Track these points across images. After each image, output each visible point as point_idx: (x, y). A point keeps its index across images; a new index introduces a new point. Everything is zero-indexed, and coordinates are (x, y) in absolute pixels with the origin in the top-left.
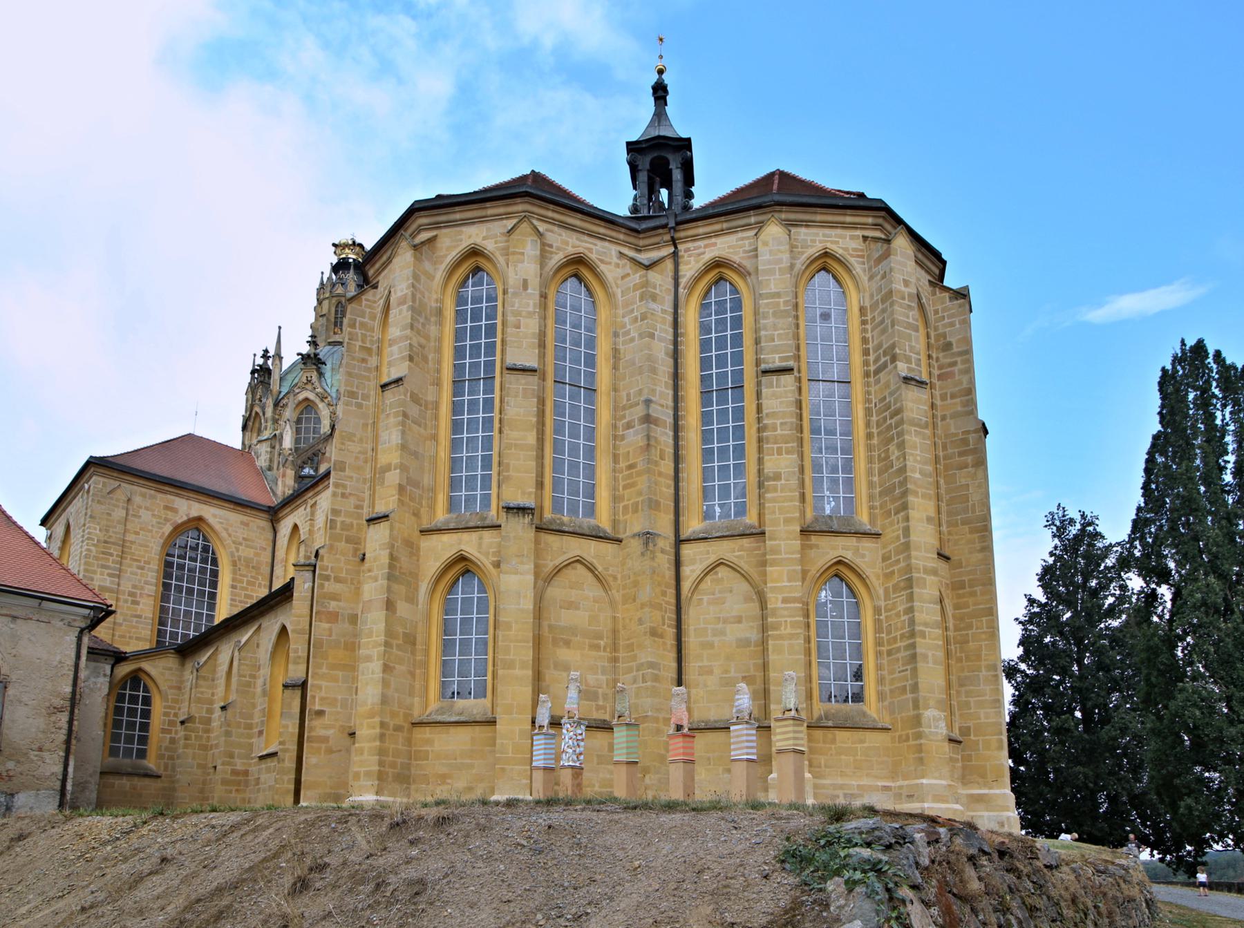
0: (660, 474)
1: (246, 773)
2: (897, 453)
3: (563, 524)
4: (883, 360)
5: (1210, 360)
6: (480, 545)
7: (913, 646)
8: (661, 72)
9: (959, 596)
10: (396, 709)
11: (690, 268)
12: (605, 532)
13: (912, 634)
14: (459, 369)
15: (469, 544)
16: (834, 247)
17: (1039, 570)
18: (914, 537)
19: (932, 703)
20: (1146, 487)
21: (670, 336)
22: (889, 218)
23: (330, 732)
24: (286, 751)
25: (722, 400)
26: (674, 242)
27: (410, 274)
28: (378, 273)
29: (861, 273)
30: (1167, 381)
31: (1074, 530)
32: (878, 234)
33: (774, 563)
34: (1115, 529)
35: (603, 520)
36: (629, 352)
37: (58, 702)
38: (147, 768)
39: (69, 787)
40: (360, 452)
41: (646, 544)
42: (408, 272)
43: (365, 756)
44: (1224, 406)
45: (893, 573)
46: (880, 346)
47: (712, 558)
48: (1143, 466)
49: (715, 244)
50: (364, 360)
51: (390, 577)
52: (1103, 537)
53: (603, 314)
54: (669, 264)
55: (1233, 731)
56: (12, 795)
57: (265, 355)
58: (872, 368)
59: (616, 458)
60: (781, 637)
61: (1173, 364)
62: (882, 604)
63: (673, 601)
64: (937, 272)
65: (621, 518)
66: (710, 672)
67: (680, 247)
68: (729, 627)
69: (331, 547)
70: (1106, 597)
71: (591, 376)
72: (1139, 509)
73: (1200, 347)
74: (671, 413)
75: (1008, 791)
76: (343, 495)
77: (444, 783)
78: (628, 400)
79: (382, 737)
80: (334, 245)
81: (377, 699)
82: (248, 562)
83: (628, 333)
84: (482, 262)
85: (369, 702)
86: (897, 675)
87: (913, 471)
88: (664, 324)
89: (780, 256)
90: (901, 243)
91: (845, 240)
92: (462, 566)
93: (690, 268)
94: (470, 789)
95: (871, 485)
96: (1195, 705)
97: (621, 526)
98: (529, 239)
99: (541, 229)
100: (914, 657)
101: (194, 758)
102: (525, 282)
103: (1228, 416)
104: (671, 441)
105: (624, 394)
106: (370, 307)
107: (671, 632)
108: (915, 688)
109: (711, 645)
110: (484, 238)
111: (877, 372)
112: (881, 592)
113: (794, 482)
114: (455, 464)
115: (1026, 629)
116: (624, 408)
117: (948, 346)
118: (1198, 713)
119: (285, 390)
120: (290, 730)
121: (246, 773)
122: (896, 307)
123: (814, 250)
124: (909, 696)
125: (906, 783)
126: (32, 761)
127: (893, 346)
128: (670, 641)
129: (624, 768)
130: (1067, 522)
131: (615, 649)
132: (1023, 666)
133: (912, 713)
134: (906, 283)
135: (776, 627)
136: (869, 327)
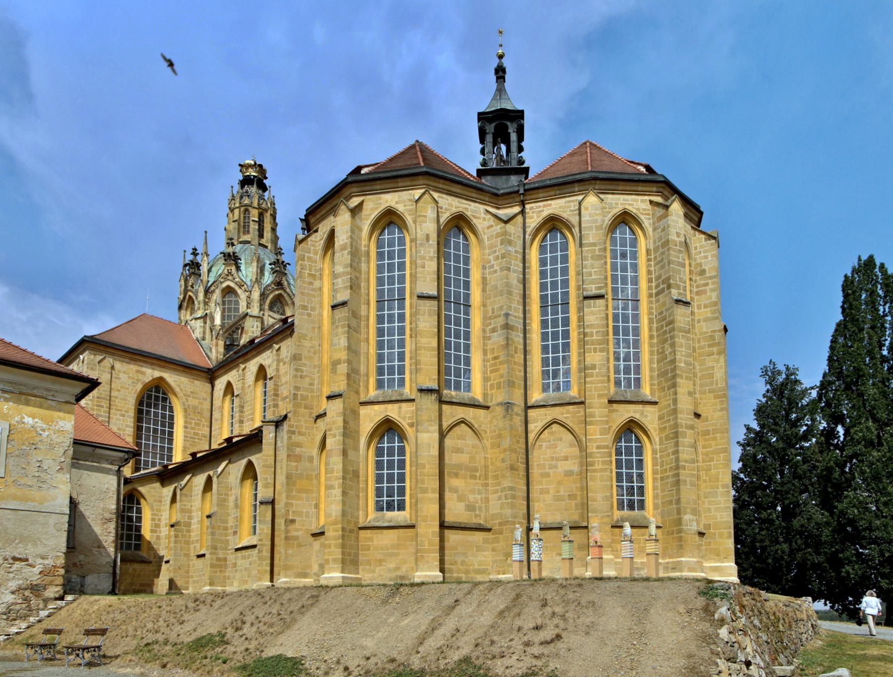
0: (515, 363)
1: (225, 559)
2: (670, 350)
3: (452, 397)
4: (662, 286)
5: (877, 270)
6: (400, 412)
7: (678, 475)
9: (706, 440)
10: (350, 518)
12: (479, 402)
13: (677, 467)
14: (380, 293)
15: (393, 412)
16: (630, 208)
17: (755, 408)
18: (680, 406)
19: (688, 510)
20: (830, 359)
22: (666, 187)
23: (299, 533)
24: (262, 545)
27: (349, 229)
29: (648, 226)
30: (848, 286)
31: (781, 378)
32: (659, 199)
33: (591, 423)
34: (812, 375)
36: (493, 279)
37: (107, 515)
38: (142, 557)
39: (118, 571)
40: (311, 347)
41: (507, 410)
42: (348, 227)
43: (333, 549)
44: (885, 304)
45: (665, 427)
47: (549, 418)
48: (829, 344)
49: (550, 205)
50: (311, 283)
51: (345, 435)
52: (801, 384)
55: (878, 522)
56: (84, 577)
57: (195, 253)
58: (654, 291)
59: (485, 352)
60: (595, 471)
61: (852, 274)
63: (524, 446)
64: (697, 219)
65: (489, 392)
66: (548, 492)
67: (527, 206)
68: (560, 463)
69: (295, 412)
70: (801, 426)
71: (467, 296)
72: (825, 375)
73: (870, 261)
74: (522, 321)
75: (733, 564)
76: (301, 377)
77: (380, 565)
78: (493, 313)
79: (343, 536)
80: (240, 165)
81: (339, 513)
82: (195, 408)
83: (492, 266)
84: (395, 219)
85: (334, 514)
86: (666, 493)
87: (680, 362)
88: (516, 260)
89: (596, 217)
90: (676, 207)
91: (638, 204)
92: (388, 428)
94: (397, 568)
95: (651, 370)
96: (854, 506)
97: (489, 397)
98: (429, 206)
99: (436, 197)
100: (678, 482)
101: (181, 550)
102: (428, 235)
103: (887, 310)
104: (522, 341)
105: (490, 308)
106: (314, 246)
107: (522, 466)
108: (678, 501)
109: (548, 475)
110: (397, 203)
112: (657, 439)
113: (604, 370)
114: (380, 358)
115: (744, 450)
116: (490, 318)
117: (703, 272)
118: (856, 511)
119: (211, 280)
120: (265, 531)
122: (672, 252)
123: (617, 210)
124: (675, 506)
125: (671, 560)
126: (94, 555)
128: (522, 473)
129: (568, 561)
130: (776, 372)
131: (486, 478)
132: (742, 476)
133: (676, 517)
134: (678, 234)
135: (592, 464)
136: (652, 263)
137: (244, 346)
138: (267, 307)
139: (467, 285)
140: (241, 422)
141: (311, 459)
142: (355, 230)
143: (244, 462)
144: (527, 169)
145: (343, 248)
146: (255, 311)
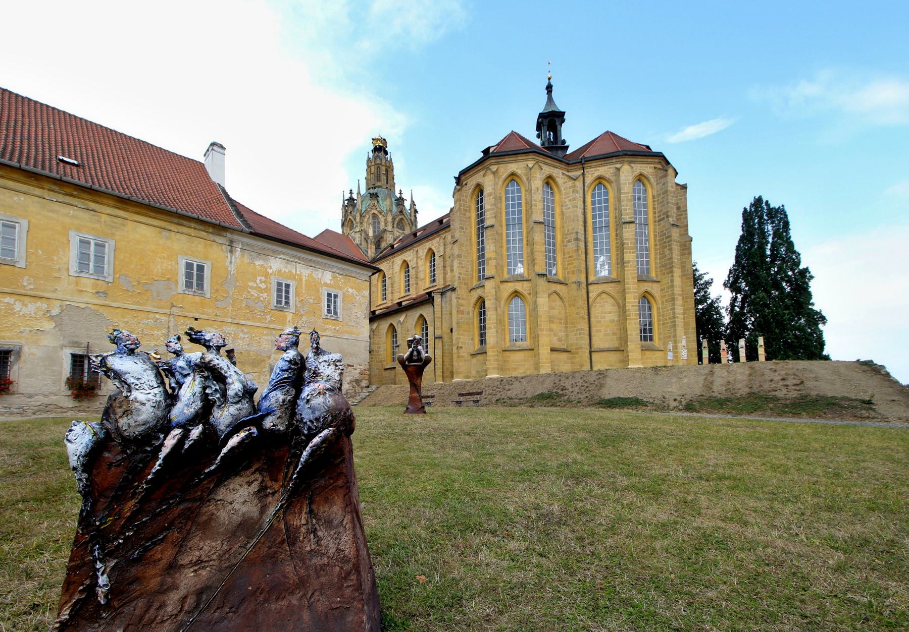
8: (549, 79)
11: (589, 179)
13: (674, 317)
14: (507, 220)
15: (519, 286)
18: (675, 283)
20: (737, 257)
25: (601, 231)
28: (467, 179)
30: (747, 216)
32: (659, 166)
35: (560, 277)
47: (600, 290)
51: (496, 299)
53: (557, 197)
54: (581, 178)
66: (600, 331)
84: (515, 178)
91: (647, 168)
93: (589, 179)
95: (656, 263)
109: (600, 322)
111: (659, 221)
119: (364, 210)
128: (587, 321)
135: (629, 315)
141: (468, 313)
142: (496, 184)
143: (417, 315)
144: (567, 147)
145: (490, 195)
146: (389, 228)
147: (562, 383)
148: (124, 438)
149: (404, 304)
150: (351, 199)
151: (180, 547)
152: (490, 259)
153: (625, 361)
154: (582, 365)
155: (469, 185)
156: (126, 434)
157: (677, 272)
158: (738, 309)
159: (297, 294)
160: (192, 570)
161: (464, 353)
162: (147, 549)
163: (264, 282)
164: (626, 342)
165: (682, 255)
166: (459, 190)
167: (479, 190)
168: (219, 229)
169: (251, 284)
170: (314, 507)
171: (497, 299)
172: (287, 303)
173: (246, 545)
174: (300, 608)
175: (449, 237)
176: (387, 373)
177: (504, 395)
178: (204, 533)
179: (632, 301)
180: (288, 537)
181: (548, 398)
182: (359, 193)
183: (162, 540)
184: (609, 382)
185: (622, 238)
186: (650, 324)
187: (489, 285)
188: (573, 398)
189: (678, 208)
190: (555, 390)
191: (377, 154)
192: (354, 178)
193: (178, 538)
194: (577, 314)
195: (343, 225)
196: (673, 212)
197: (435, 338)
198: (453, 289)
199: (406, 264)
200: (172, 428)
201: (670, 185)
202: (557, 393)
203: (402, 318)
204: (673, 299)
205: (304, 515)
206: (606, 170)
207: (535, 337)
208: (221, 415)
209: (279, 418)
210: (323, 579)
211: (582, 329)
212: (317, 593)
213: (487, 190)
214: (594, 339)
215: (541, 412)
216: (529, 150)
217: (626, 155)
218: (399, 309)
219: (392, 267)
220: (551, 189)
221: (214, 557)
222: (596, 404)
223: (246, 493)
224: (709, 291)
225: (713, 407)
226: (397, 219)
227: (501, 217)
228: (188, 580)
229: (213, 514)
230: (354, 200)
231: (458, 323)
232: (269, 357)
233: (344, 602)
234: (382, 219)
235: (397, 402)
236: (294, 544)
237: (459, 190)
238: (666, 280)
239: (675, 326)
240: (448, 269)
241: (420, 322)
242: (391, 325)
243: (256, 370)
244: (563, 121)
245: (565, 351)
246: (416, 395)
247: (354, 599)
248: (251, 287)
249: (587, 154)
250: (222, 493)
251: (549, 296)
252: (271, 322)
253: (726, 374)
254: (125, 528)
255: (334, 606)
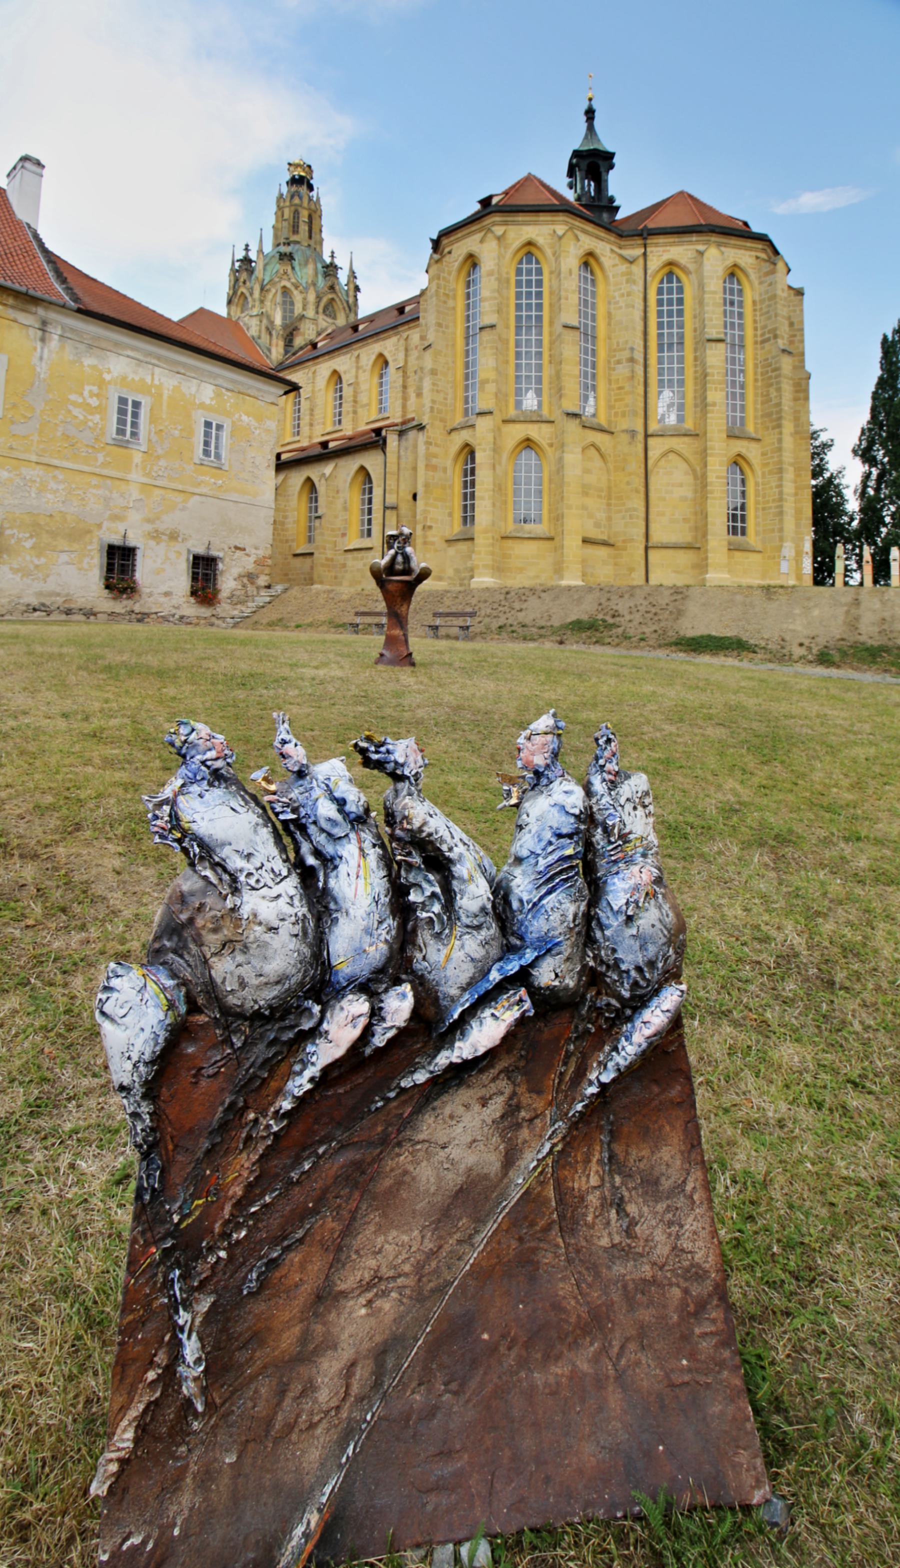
11: (654, 263)
13: (781, 499)
14: (519, 318)
15: (533, 431)
21: (641, 307)
23: (435, 539)
26: (645, 246)
32: (763, 256)
35: (602, 420)
46: (764, 327)
47: (667, 447)
53: (601, 288)
54: (641, 261)
59: (610, 382)
62: (760, 480)
84: (533, 250)
91: (745, 256)
93: (654, 263)
94: (537, 577)
95: (756, 410)
107: (642, 489)
111: (763, 342)
114: (518, 378)
121: (332, 560)
127: (775, 329)
128: (642, 496)
137: (301, 348)
138: (321, 310)
139: (594, 319)
140: (311, 425)
141: (445, 470)
142: (500, 257)
144: (617, 209)
145: (490, 274)
146: (310, 313)
147: (612, 605)
148: (226, 1011)
149: (331, 445)
150: (247, 261)
151: (338, 1252)
152: (484, 382)
153: (702, 566)
154: (632, 570)
155: (454, 254)
156: (232, 1000)
157: (788, 427)
158: (871, 492)
159: (153, 420)
160: (363, 1300)
161: (435, 536)
162: (273, 1264)
163: (97, 395)
164: (705, 535)
165: (796, 399)
166: (437, 262)
167: (472, 262)
168: (27, 300)
169: (73, 397)
170: (618, 1149)
171: (496, 449)
172: (134, 434)
173: (471, 1237)
174: (600, 1382)
175: (414, 335)
176: (298, 561)
177: (513, 618)
178: (384, 1215)
179: (717, 468)
180: (562, 1217)
181: (589, 629)
182: (260, 251)
183: (301, 1241)
184: (693, 608)
185: (704, 364)
186: (743, 508)
187: (484, 425)
188: (631, 632)
189: (791, 324)
190: (600, 617)
191: (294, 188)
192: (254, 227)
193: (332, 1231)
194: (628, 483)
195: (230, 302)
196: (784, 329)
197: (386, 508)
198: (421, 428)
199: (336, 377)
200: (339, 993)
201: (779, 286)
202: (604, 621)
203: (328, 468)
204: (780, 471)
205: (594, 1166)
206: (679, 251)
207: (558, 518)
208: (448, 958)
209: (568, 959)
210: (646, 1315)
211: (635, 510)
212: (632, 1346)
213: (487, 263)
214: (653, 526)
215: (579, 653)
216: (561, 208)
217: (713, 231)
218: (324, 453)
219: (313, 379)
220: (592, 273)
221: (407, 1268)
222: (670, 645)
223: (477, 1123)
224: (827, 458)
225: (862, 660)
226: (325, 300)
227: (508, 313)
228: (357, 1324)
229: (406, 1172)
230: (251, 261)
231: (427, 485)
232: (100, 526)
233: (697, 1371)
234: (297, 297)
235: (322, 618)
236: (573, 1232)
237: (437, 262)
238: (770, 439)
239: (781, 513)
240: (411, 392)
241: (360, 478)
242: (309, 479)
243: (76, 546)
244: (612, 167)
245: (605, 544)
246: (397, 632)
247: (722, 1364)
248: (75, 404)
249: (651, 224)
250: (429, 1126)
251: (584, 449)
252: (105, 465)
253: (878, 606)
254: (233, 1224)
255: (677, 1378)
